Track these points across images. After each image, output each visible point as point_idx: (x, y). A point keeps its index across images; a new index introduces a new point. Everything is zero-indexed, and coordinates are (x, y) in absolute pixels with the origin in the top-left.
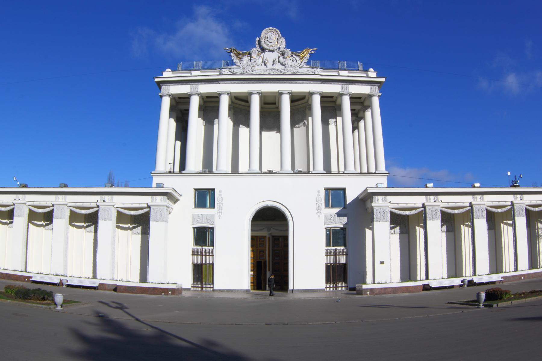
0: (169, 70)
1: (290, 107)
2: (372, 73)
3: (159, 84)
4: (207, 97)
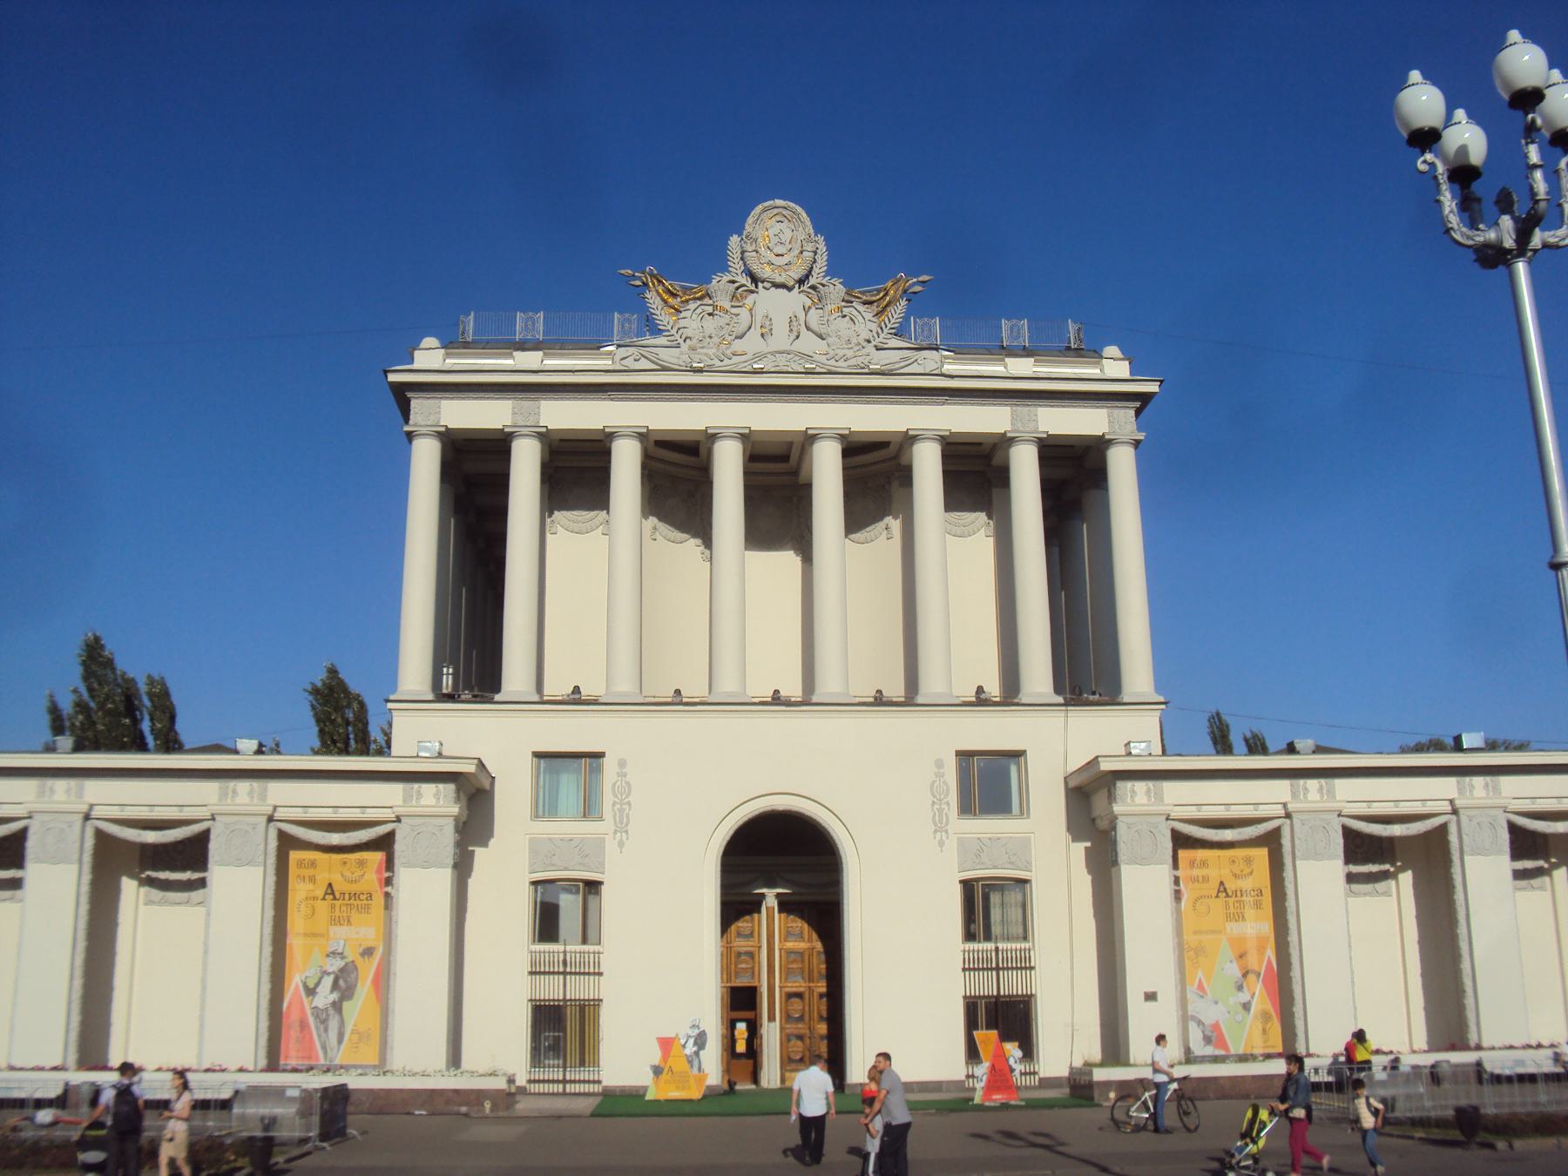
1: (845, 469)
2: (1114, 368)
3: (402, 395)
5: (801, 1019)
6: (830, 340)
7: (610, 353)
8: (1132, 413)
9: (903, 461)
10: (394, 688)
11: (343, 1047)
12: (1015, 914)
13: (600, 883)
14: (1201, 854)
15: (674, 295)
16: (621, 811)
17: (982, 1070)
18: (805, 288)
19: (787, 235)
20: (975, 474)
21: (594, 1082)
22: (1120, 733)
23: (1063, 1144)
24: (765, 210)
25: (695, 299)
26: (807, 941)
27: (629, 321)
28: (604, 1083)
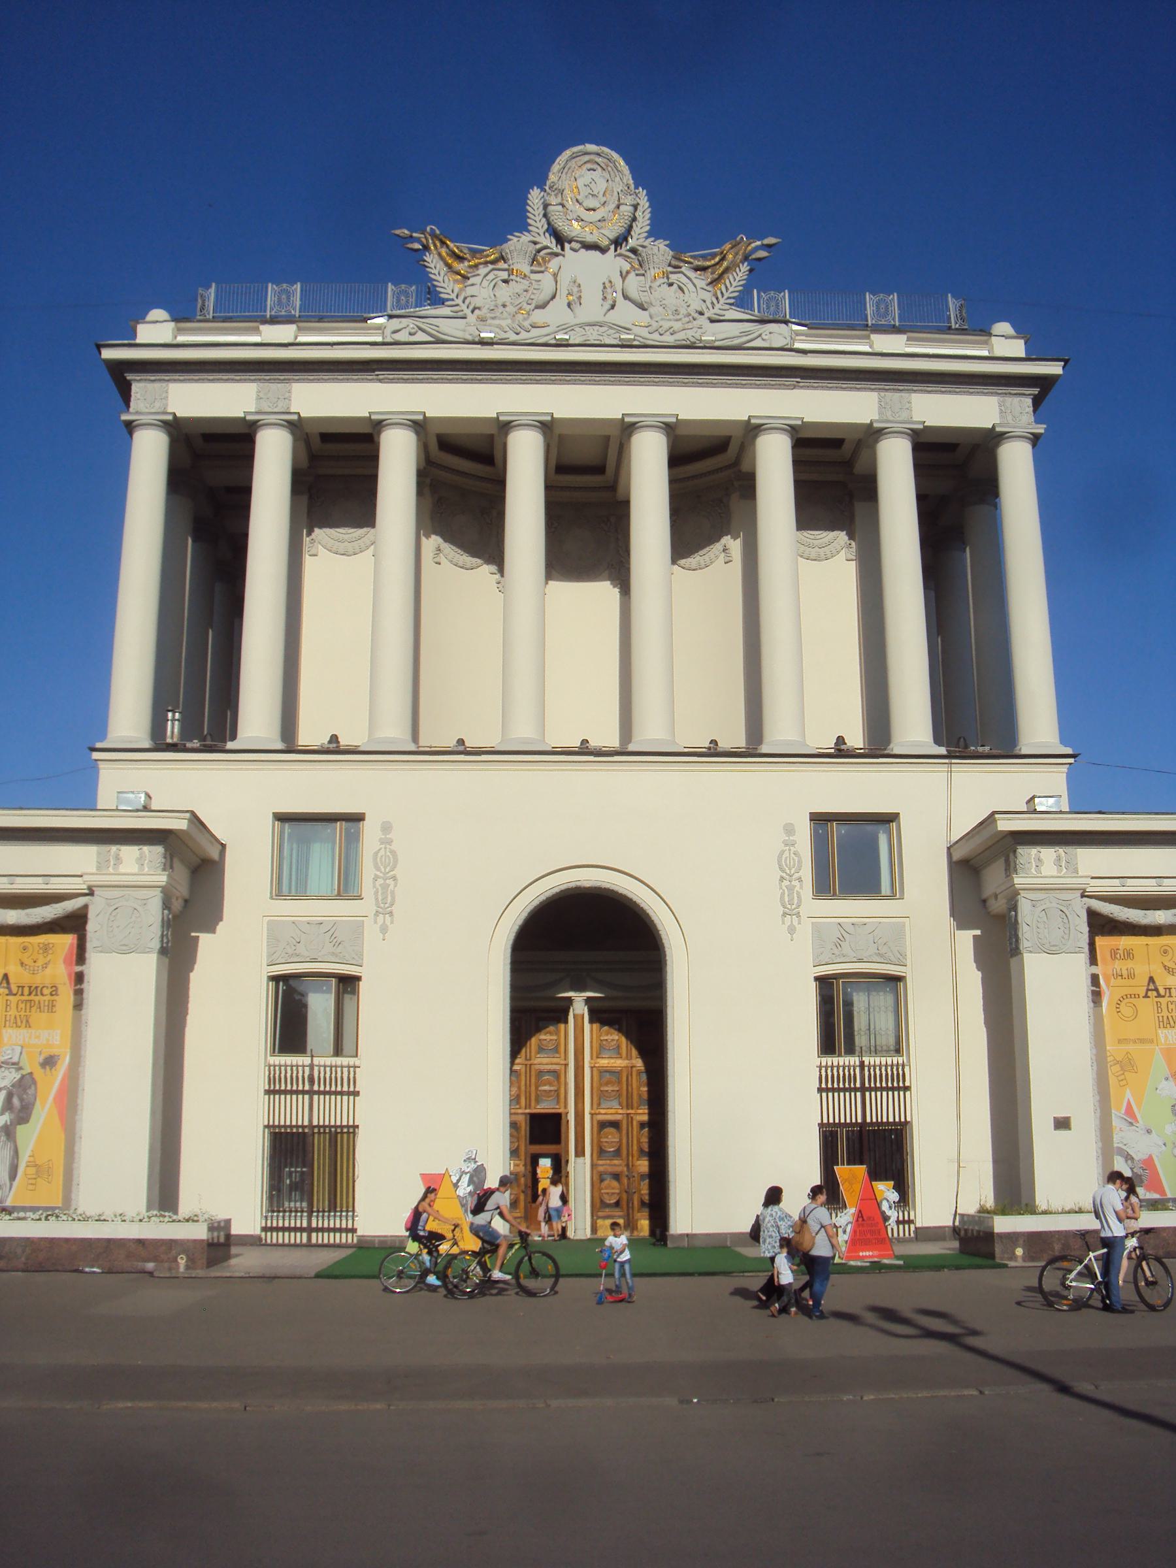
0: (158, 314)
1: (672, 481)
2: (1006, 345)
4: (326, 437)
5: (617, 1153)
6: (652, 310)
7: (379, 328)
8: (1029, 401)
9: (745, 467)
10: (103, 736)
11: (15, 1183)
12: (884, 1023)
13: (358, 979)
14: (1125, 942)
15: (460, 259)
16: (385, 887)
17: (845, 1219)
18: (623, 250)
19: (601, 185)
20: (834, 480)
21: (347, 1230)
22: (1020, 791)
23: (975, 1333)
24: (572, 157)
25: (486, 263)
26: (626, 1060)
27: (407, 294)
28: (359, 1233)
